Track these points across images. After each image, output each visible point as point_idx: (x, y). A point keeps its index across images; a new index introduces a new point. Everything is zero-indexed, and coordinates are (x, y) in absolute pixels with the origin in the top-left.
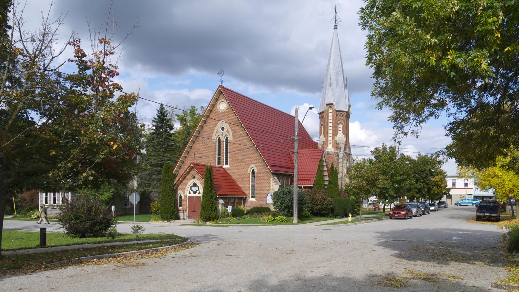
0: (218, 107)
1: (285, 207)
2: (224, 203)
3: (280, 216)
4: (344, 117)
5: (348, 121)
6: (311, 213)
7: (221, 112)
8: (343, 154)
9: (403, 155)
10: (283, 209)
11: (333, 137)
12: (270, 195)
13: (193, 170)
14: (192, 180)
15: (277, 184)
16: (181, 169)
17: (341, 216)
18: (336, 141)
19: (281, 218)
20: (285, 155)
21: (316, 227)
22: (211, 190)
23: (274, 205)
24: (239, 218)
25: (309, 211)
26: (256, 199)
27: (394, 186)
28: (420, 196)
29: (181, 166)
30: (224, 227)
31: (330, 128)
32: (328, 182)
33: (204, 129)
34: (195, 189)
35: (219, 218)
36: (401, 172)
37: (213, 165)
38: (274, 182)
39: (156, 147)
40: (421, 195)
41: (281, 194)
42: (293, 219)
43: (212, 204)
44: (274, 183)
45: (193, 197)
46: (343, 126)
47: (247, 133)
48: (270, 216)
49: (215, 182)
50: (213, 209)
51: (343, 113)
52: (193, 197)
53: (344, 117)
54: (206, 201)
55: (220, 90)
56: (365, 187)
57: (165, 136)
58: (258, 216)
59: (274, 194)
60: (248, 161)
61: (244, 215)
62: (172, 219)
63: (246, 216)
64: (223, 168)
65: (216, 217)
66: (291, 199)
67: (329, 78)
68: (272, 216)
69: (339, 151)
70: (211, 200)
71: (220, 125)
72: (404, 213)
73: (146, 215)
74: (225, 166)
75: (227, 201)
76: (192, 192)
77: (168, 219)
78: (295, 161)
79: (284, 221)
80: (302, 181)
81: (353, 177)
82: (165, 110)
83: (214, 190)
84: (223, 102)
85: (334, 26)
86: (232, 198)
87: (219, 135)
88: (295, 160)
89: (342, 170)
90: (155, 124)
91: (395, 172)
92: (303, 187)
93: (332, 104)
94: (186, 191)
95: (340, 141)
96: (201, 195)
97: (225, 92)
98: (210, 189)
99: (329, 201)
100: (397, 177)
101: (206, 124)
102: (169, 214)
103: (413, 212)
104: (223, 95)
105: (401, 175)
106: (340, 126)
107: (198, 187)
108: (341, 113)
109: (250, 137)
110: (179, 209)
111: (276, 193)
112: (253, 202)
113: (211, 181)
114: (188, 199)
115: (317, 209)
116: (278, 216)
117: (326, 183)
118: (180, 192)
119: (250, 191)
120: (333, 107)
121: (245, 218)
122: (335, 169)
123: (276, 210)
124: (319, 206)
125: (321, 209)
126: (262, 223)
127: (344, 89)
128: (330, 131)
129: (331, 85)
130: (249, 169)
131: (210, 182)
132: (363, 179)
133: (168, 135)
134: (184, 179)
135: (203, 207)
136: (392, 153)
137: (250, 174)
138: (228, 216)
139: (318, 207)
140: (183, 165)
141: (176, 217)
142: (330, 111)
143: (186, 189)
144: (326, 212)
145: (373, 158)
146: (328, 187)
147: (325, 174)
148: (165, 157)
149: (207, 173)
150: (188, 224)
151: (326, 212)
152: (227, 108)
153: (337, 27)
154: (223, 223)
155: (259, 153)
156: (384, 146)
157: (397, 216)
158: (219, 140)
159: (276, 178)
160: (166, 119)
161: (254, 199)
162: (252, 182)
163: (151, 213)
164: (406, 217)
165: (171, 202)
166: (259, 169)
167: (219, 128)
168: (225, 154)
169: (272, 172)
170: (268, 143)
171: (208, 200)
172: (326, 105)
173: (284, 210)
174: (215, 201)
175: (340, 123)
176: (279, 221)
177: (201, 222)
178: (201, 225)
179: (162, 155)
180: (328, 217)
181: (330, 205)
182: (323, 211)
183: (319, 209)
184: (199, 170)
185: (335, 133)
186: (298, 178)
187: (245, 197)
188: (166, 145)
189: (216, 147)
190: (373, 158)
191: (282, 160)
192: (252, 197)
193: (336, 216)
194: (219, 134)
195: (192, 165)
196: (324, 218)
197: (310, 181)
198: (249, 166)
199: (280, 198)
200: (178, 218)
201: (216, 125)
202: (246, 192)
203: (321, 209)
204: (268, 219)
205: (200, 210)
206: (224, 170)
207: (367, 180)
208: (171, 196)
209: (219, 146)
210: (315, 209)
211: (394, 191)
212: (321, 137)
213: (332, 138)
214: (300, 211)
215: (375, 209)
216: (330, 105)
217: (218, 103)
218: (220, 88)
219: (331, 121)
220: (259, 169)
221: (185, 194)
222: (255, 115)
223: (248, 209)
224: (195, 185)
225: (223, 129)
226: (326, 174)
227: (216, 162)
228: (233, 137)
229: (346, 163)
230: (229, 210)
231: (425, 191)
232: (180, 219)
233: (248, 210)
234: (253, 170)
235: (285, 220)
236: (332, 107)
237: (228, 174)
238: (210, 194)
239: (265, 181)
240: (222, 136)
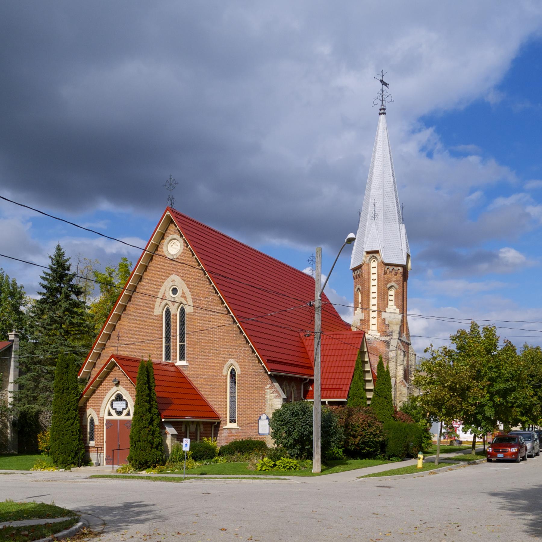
0: (165, 249)
1: (295, 440)
2: (176, 433)
3: (287, 458)
4: (399, 275)
5: (405, 283)
6: (344, 452)
8: (398, 343)
9: (510, 343)
10: (291, 445)
12: (266, 417)
13: (116, 368)
14: (115, 388)
15: (279, 396)
17: (400, 458)
19: (288, 462)
20: (295, 344)
21: (359, 480)
22: (150, 409)
23: (274, 437)
24: (205, 462)
25: (339, 448)
26: (238, 425)
27: (494, 401)
28: (528, 419)
29: (95, 363)
30: (174, 480)
31: (372, 295)
32: (372, 393)
34: (119, 406)
35: (167, 463)
36: (507, 375)
37: (154, 360)
38: (273, 393)
39: (48, 327)
40: (529, 417)
41: (287, 416)
42: (312, 464)
43: (152, 435)
44: (274, 395)
45: (117, 420)
46: (397, 292)
47: (221, 299)
48: (266, 459)
49: (157, 392)
50: (154, 446)
51: (396, 268)
52: (115, 421)
53: (399, 275)
54: (141, 429)
55: (168, 217)
56: (448, 401)
57: (65, 305)
58: (243, 458)
59: (274, 414)
60: (222, 353)
61: (215, 456)
62: (75, 464)
63: (220, 459)
64: (176, 366)
65: (159, 460)
66: (307, 424)
67: (370, 204)
68: (270, 458)
69: (389, 337)
70: (151, 427)
72: (514, 450)
73: (29, 457)
74: (179, 363)
75: (183, 430)
77: (66, 465)
78: (317, 349)
79: (295, 469)
80: (329, 392)
81: (424, 382)
82: (65, 258)
83: (157, 408)
84: (174, 239)
85: (381, 110)
86: (193, 422)
87: (166, 304)
88: (316, 347)
89: (396, 371)
90: (45, 283)
91: (497, 375)
92: (327, 403)
93: (377, 252)
94: (102, 410)
95: (391, 319)
96: (131, 418)
97: (179, 220)
98: (148, 406)
99: (378, 428)
100: (501, 385)
102: (69, 456)
103: (528, 448)
104: (174, 226)
105: (508, 380)
106: (392, 292)
107: (125, 402)
108: (393, 267)
109: (226, 307)
110: (90, 445)
111: (277, 414)
112: (233, 431)
113: (150, 389)
114: (106, 425)
115: (356, 443)
116: (282, 458)
117: (370, 395)
118: (90, 412)
119: (226, 410)
120: (378, 257)
121: (217, 461)
122: (385, 369)
123: (278, 445)
124: (359, 438)
125: (363, 443)
126: (250, 473)
127: (398, 224)
128: (374, 301)
129: (374, 217)
131: (148, 392)
132: (444, 387)
133: (70, 304)
134: (98, 387)
135: (135, 442)
136: (491, 340)
137: (226, 378)
138: (183, 459)
139: (357, 440)
140: (99, 360)
141: (82, 460)
142: (374, 264)
143: (103, 405)
144: (371, 450)
145: (453, 347)
146: (372, 403)
147: (367, 379)
148: (65, 345)
149: (141, 374)
150: (107, 474)
151: (371, 450)
153: (386, 111)
154: (173, 472)
155: (244, 336)
156: (474, 327)
157: (500, 455)
158: (168, 312)
159: (277, 384)
160: (67, 275)
161: (234, 426)
162: (231, 393)
163: (39, 452)
164: (517, 458)
165: (72, 432)
166: (245, 368)
167: (167, 290)
169: (269, 373)
170: (264, 315)
171: (145, 427)
173: (293, 446)
174: (158, 429)
175: (391, 287)
176: (284, 467)
177: (131, 472)
178: (129, 477)
179: (59, 341)
180: (374, 459)
181: (379, 437)
182: (367, 448)
183: (358, 443)
184: (129, 369)
185: (383, 305)
186: (322, 385)
187: (218, 421)
188: (68, 324)
189: (162, 327)
190: (453, 347)
191: (303, 316)
192: (230, 422)
193: (389, 457)
195: (113, 360)
196: (367, 461)
197: (339, 392)
198: (226, 362)
199: (286, 424)
200: (86, 462)
201: (161, 285)
202: (219, 411)
203: (363, 443)
204: (263, 465)
205: (129, 446)
206: (178, 370)
207: (452, 389)
208: (72, 421)
209: (168, 324)
210: (352, 444)
211: (493, 409)
212: (356, 312)
214: (325, 447)
215: (451, 443)
216: (373, 253)
217: (166, 241)
218: (168, 213)
219: (375, 283)
220: (245, 368)
221: (101, 416)
222: (236, 266)
223: (224, 443)
224: (119, 398)
225: (175, 291)
226: (369, 377)
227: (162, 355)
229: (402, 359)
230: (184, 446)
231: (536, 411)
232: (92, 465)
233: (223, 446)
235: (295, 465)
236: (376, 258)
237: (184, 377)
238: (148, 416)
239: (256, 391)
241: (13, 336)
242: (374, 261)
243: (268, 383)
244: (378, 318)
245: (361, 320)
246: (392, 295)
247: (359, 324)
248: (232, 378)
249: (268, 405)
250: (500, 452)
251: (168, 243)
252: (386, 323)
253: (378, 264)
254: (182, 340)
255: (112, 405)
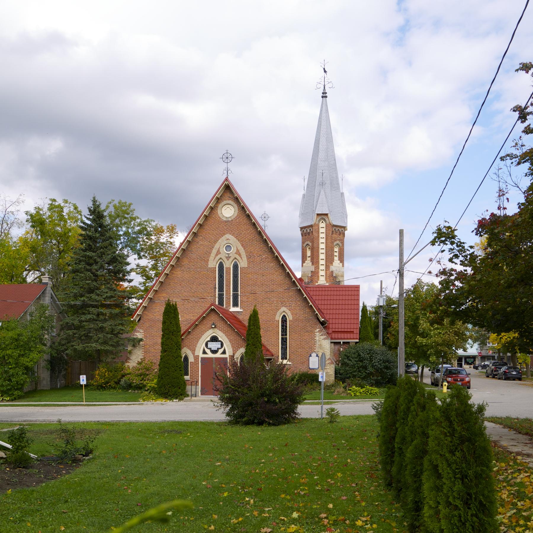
7: (226, 222)
11: (326, 265)
12: (316, 355)
16: (146, 312)
18: (332, 272)
31: (321, 251)
33: (194, 247)
34: (214, 346)
38: (322, 335)
44: (322, 337)
52: (210, 359)
71: (221, 243)
74: (233, 309)
76: (209, 350)
84: (228, 204)
87: (221, 258)
92: (342, 343)
93: (327, 215)
94: (197, 349)
95: (337, 272)
101: (197, 239)
107: (220, 343)
118: (185, 351)
120: (327, 219)
128: (322, 256)
130: (278, 314)
142: (322, 225)
152: (236, 215)
158: (221, 266)
162: (282, 335)
166: (296, 315)
168: (217, 290)
172: (316, 215)
185: (329, 260)
194: (222, 256)
198: (278, 310)
201: (215, 242)
202: (273, 351)
209: (221, 276)
212: (304, 264)
213: (326, 267)
216: (323, 216)
217: (220, 206)
224: (214, 339)
225: (228, 248)
228: (249, 263)
234: (284, 316)
239: (307, 334)
240: (228, 260)
241: (47, 279)
242: (322, 222)
243: (318, 327)
244: (326, 270)
245: (312, 272)
246: (336, 252)
247: (310, 275)
248: (284, 323)
249: (317, 345)
250: (458, 381)
251: (223, 207)
252: (334, 275)
253: (326, 225)
254: (235, 289)
255: (207, 345)
